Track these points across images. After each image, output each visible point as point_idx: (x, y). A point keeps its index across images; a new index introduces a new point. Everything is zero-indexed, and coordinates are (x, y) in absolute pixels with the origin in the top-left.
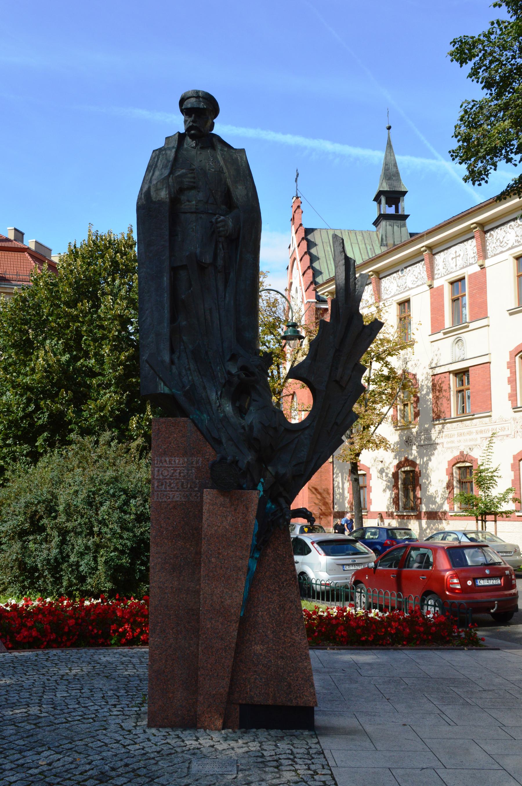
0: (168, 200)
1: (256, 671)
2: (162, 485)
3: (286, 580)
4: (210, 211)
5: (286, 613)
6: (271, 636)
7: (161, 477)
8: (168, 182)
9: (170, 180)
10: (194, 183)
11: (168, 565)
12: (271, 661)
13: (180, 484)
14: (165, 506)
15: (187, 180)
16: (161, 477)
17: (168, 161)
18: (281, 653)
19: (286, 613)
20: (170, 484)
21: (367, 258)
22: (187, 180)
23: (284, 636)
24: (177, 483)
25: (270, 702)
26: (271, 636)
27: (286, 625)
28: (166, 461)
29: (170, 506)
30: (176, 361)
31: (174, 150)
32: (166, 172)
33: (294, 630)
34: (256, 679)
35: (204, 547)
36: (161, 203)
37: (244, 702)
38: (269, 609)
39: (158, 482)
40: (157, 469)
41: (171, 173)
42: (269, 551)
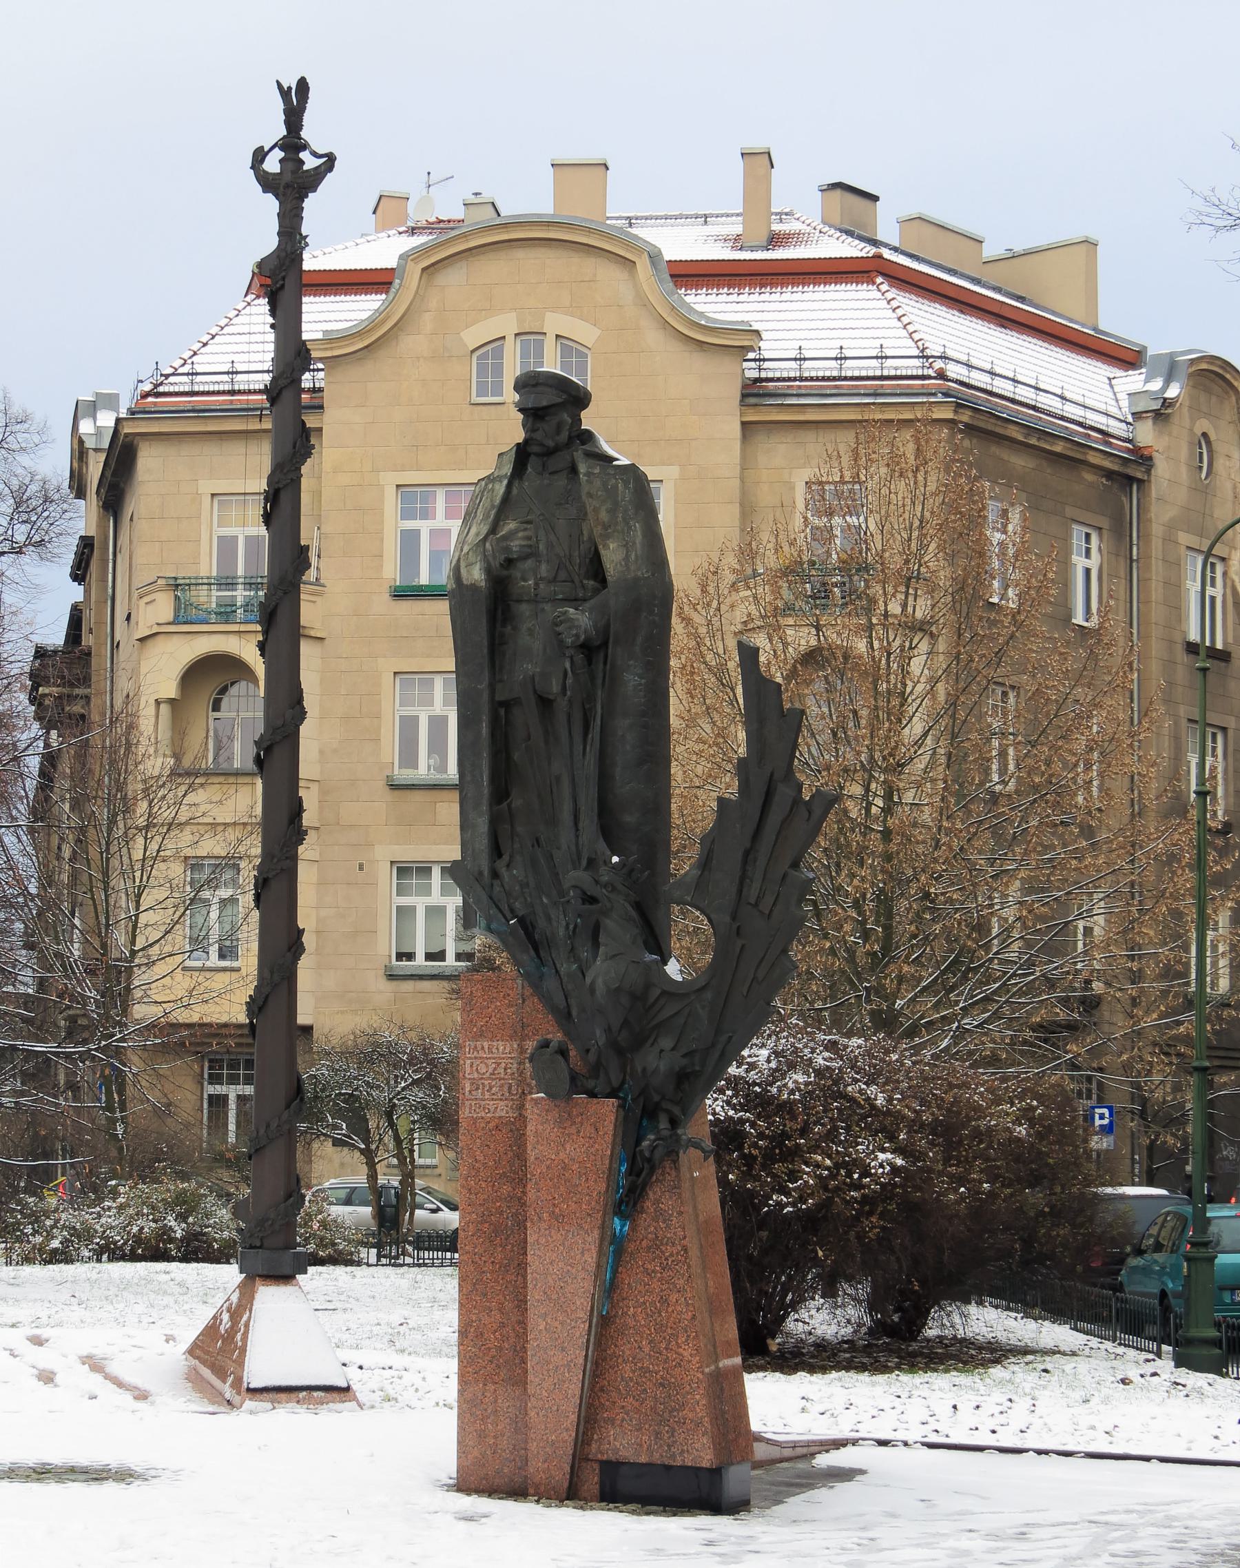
0: (483, 584)
1: (623, 1407)
2: (477, 1089)
3: (672, 1255)
4: (560, 596)
5: (670, 1310)
6: (647, 1350)
7: (476, 1075)
8: (485, 550)
9: (488, 545)
10: (530, 546)
11: (486, 1225)
12: (645, 1390)
13: (506, 1088)
14: (483, 1125)
15: (517, 543)
16: (476, 1075)
17: (493, 506)
18: (662, 1377)
19: (670, 1310)
20: (491, 1088)
21: (449, 810)
22: (517, 543)
23: (666, 1349)
24: (502, 1086)
25: (643, 1459)
26: (647, 1350)
27: (669, 1331)
28: (483, 1048)
29: (491, 1125)
30: (503, 871)
31: (505, 482)
32: (485, 529)
33: (681, 1340)
34: (623, 1420)
35: (531, 1194)
36: (474, 587)
37: (605, 1458)
38: (644, 1303)
39: (472, 1084)
40: (468, 1062)
41: (493, 530)
42: (648, 1204)
